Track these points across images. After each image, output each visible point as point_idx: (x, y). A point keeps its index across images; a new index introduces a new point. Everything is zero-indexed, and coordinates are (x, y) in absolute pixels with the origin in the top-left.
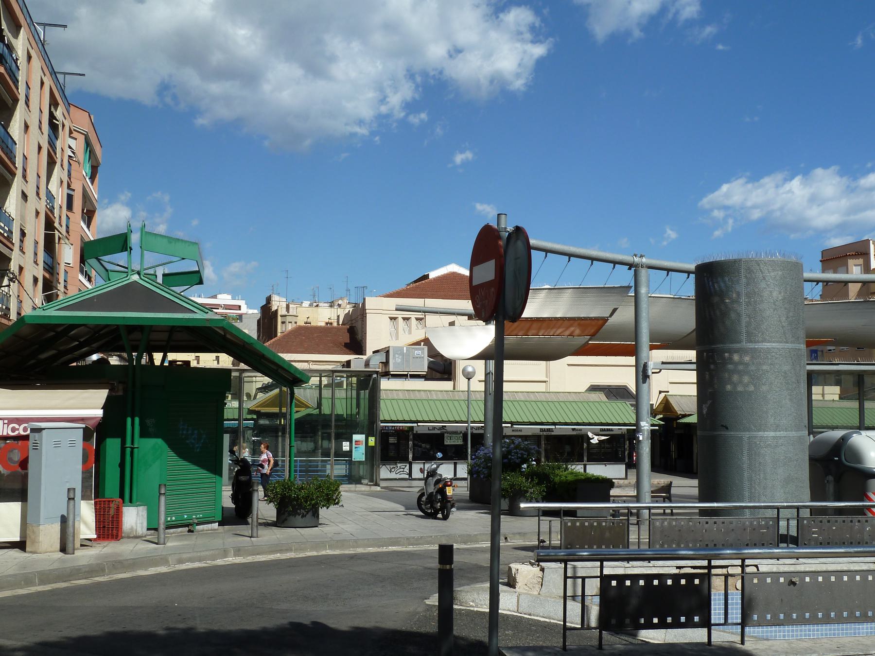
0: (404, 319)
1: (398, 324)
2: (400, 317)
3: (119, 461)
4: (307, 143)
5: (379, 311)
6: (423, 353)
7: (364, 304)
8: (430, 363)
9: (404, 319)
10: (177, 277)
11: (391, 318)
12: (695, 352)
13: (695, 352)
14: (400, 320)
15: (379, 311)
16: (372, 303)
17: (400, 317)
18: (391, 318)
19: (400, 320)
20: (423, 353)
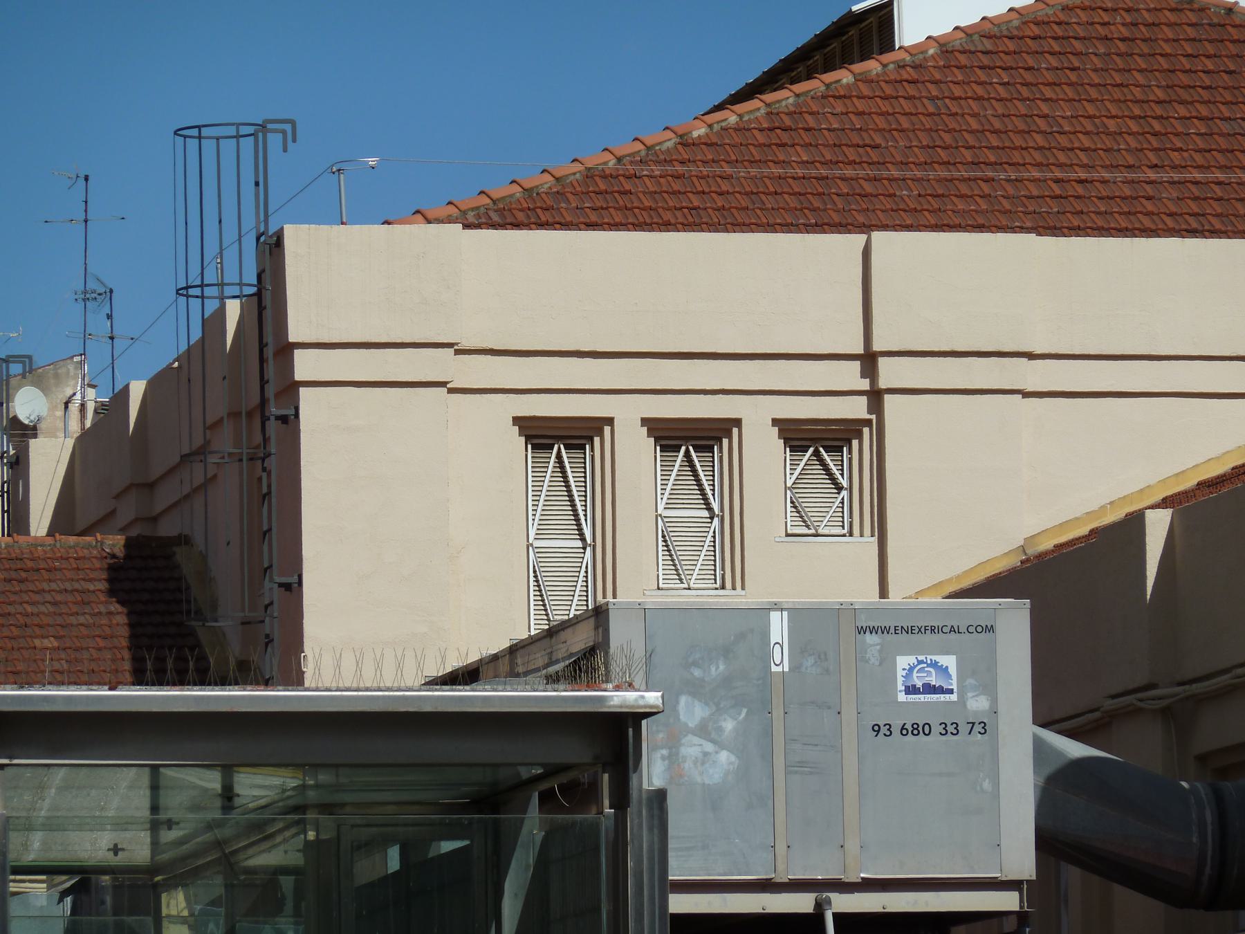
0: (670, 436)
1: (604, 493)
2: (628, 417)
3: (1025, 360)
4: (1158, 526)
5: (422, 366)
6: (982, 674)
7: (267, 299)
8: (1060, 787)
9: (670, 436)
10: (207, 394)
11: (541, 435)
12: (671, 896)
13: (671, 896)
14: (633, 451)
15: (422, 366)
16: (339, 279)
17: (628, 417)
18: (541, 435)
19: (633, 451)
20: (982, 674)
